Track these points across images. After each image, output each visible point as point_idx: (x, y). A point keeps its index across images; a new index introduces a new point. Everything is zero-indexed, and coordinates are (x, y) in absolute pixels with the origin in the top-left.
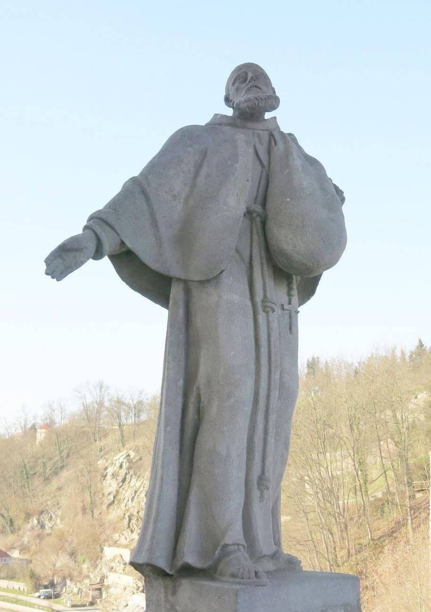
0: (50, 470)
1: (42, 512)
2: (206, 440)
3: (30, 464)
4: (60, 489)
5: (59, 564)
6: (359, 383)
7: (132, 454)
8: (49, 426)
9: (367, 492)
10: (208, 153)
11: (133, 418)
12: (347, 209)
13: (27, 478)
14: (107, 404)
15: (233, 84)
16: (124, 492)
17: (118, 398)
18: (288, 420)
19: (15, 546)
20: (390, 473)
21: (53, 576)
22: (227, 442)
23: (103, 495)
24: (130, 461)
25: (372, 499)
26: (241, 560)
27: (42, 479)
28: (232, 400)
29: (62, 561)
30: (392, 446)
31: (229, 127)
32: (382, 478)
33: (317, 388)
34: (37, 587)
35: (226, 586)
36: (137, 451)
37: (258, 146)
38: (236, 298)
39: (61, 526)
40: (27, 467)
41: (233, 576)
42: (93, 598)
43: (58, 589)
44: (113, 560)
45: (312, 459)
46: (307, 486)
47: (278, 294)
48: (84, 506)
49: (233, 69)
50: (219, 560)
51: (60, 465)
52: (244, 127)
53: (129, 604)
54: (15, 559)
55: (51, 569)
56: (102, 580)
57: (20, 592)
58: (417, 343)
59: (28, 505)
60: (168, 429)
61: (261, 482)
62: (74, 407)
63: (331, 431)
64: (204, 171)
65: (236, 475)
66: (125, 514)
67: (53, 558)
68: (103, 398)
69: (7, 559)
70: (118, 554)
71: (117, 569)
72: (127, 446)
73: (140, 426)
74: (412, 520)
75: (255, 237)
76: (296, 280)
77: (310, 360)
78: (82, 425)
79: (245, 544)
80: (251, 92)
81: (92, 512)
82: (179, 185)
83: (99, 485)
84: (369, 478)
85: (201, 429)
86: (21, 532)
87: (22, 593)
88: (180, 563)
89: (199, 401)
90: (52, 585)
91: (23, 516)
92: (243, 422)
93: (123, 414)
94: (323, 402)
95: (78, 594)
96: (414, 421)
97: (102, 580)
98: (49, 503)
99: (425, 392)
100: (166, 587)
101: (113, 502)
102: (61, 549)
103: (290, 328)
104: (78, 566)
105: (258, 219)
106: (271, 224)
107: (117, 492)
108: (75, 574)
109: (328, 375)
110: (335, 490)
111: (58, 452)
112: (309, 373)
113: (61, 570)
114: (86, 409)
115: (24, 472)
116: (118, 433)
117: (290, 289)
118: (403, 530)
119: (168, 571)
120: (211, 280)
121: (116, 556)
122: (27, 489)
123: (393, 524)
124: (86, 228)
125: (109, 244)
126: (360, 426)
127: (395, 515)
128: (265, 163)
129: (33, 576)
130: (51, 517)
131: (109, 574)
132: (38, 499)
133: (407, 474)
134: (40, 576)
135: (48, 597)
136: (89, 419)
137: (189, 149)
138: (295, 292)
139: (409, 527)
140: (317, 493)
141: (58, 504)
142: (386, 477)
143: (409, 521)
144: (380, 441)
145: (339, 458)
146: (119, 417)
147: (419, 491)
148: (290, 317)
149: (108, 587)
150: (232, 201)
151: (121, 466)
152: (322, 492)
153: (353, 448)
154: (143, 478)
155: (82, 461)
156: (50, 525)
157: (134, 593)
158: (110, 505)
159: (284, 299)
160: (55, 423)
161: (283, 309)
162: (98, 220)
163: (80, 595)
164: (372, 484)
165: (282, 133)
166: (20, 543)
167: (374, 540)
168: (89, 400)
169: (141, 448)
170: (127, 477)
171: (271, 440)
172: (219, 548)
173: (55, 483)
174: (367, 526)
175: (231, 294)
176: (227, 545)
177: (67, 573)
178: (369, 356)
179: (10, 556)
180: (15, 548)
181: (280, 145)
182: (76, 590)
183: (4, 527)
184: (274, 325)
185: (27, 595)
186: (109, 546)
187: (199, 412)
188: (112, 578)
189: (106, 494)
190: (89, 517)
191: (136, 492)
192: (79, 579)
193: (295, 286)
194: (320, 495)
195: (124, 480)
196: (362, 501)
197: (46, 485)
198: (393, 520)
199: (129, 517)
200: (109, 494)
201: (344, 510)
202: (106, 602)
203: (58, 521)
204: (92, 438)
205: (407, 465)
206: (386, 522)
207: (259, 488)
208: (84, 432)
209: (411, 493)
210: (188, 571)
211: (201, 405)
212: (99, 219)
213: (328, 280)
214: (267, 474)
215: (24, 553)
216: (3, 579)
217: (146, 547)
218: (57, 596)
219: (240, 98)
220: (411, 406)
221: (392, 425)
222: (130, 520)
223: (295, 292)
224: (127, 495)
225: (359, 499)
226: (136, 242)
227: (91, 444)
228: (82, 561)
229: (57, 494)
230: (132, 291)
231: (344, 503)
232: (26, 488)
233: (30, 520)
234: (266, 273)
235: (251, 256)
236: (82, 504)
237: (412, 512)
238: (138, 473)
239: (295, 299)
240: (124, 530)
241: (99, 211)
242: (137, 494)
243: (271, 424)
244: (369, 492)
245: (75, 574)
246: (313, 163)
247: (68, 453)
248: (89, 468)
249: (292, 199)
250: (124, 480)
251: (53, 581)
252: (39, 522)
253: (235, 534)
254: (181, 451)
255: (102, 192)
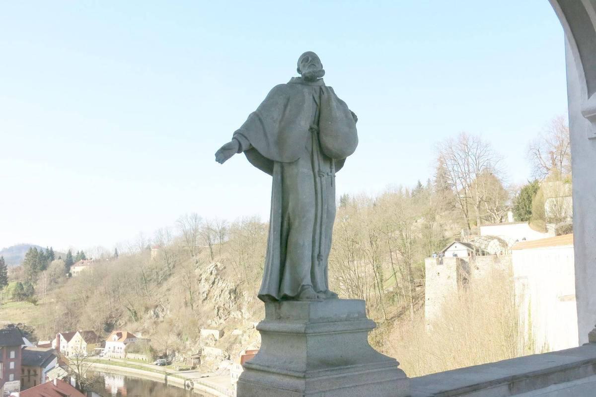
0: (162, 277)
1: (157, 306)
2: (293, 238)
3: (148, 273)
4: (169, 290)
5: (169, 342)
6: (376, 212)
7: (219, 265)
8: (160, 246)
9: (382, 287)
10: (290, 99)
11: (219, 240)
12: (358, 125)
13: (146, 283)
14: (200, 230)
15: (302, 63)
16: (214, 291)
17: (208, 226)
18: (331, 228)
19: (138, 330)
20: (399, 274)
21: (166, 349)
22: (303, 239)
23: (199, 293)
24: (217, 270)
25: (386, 292)
26: (311, 292)
27: (156, 283)
28: (305, 219)
29: (172, 339)
30: (399, 256)
31: (300, 85)
32: (393, 278)
33: (347, 216)
34: (155, 358)
35: (304, 302)
36: (222, 262)
37: (315, 96)
38: (305, 170)
39: (170, 316)
40: (145, 275)
41: (307, 298)
42: (195, 364)
43: (170, 359)
44: (207, 338)
45: (344, 265)
46: (341, 284)
47: (325, 168)
48: (186, 301)
49: (301, 54)
50: (301, 292)
51: (168, 273)
52: (308, 85)
53: (219, 368)
54: (139, 339)
55: (164, 346)
56: (200, 352)
57: (143, 361)
58: (416, 184)
59: (146, 301)
60: (275, 233)
61: (319, 257)
62: (176, 233)
63: (358, 246)
64: (289, 107)
65: (308, 253)
66: (215, 306)
67: (165, 338)
68: (198, 226)
69: (134, 339)
70: (211, 334)
71: (211, 344)
72: (215, 259)
73: (224, 245)
74: (413, 306)
75: (314, 141)
76: (334, 161)
77: (342, 196)
78: (183, 245)
79: (311, 284)
80: (311, 66)
81: (192, 305)
82: (276, 114)
83: (196, 286)
84: (384, 278)
85: (290, 233)
86: (142, 320)
87: (145, 362)
88: (282, 294)
89: (289, 220)
90: (165, 356)
91: (143, 309)
92: (310, 228)
93: (211, 237)
94: (352, 226)
95: (184, 361)
96: (415, 238)
97: (200, 352)
98: (161, 300)
99: (422, 218)
100: (275, 306)
101: (207, 298)
102: (171, 331)
103: (332, 184)
104: (183, 343)
105: (315, 133)
106: (322, 135)
107: (209, 291)
108: (181, 349)
109: (355, 207)
110: (361, 286)
111: (166, 265)
112: (341, 206)
113: (172, 346)
114: (186, 234)
115: (144, 279)
116: (209, 250)
117: (331, 165)
118: (407, 313)
119: (277, 298)
120: (294, 162)
121: (210, 335)
122: (146, 291)
123: (400, 309)
124: (233, 138)
125: (245, 146)
126: (378, 243)
127: (402, 302)
128: (319, 104)
129: (152, 350)
130: (163, 309)
131: (204, 347)
132: (154, 297)
133: (411, 274)
134: (156, 351)
135: (163, 365)
136: (188, 241)
137: (281, 97)
138: (334, 167)
139: (412, 311)
140: (348, 289)
141: (168, 300)
142: (396, 277)
143: (412, 307)
144: (391, 252)
145: (363, 264)
146: (209, 238)
147: (418, 286)
148: (332, 179)
149: (204, 356)
150: (303, 123)
151: (211, 273)
152: (352, 288)
153: (373, 257)
154: (227, 281)
155: (184, 270)
156: (163, 315)
157: (222, 360)
158: (204, 300)
159: (328, 170)
160: (164, 244)
161: (328, 175)
162: (239, 135)
163: (185, 363)
164: (386, 282)
165: (326, 87)
166: (141, 328)
167: (387, 320)
168: (188, 227)
169: (225, 260)
170: (216, 280)
171: (323, 238)
172: (300, 287)
173: (165, 286)
174: (383, 310)
175: (304, 168)
176: (303, 286)
177: (175, 348)
178: (384, 193)
179: (135, 337)
180: (138, 331)
181: (326, 93)
182: (182, 359)
183: (131, 317)
184: (324, 183)
185: (148, 364)
186: (204, 328)
187: (289, 225)
188: (207, 351)
189: (201, 292)
190: (190, 308)
191: (222, 291)
192: (184, 352)
193: (333, 164)
194: (350, 290)
195: (213, 283)
196: (379, 294)
197: (159, 287)
198: (400, 306)
199: (217, 308)
200: (203, 293)
201: (367, 300)
202: (204, 367)
203: (168, 312)
204: (191, 254)
205: (410, 268)
206: (396, 308)
207: (318, 260)
208: (185, 250)
209: (413, 288)
210: (286, 298)
211: (290, 221)
212: (240, 134)
213: (349, 160)
214: (321, 254)
215: (145, 335)
216: (131, 353)
217: (267, 287)
218: (169, 363)
219: (306, 71)
220: (412, 228)
221: (399, 241)
222: (218, 310)
223: (334, 167)
224: (216, 293)
225: (377, 291)
226: (257, 143)
227: (190, 258)
228: (186, 339)
229: (167, 293)
230: (250, 164)
231: (367, 296)
232: (145, 290)
233: (149, 312)
234: (320, 158)
235: (312, 149)
236: (184, 300)
237: (414, 300)
238: (223, 278)
239: (334, 170)
240: (214, 317)
241: (239, 130)
242: (223, 292)
243: (323, 230)
244: (384, 288)
245: (181, 348)
246: (342, 103)
247: (174, 265)
248: (189, 275)
249: (331, 122)
250: (213, 283)
251: (166, 353)
252: (155, 313)
253: (307, 281)
254: (281, 244)
255: (239, 121)
